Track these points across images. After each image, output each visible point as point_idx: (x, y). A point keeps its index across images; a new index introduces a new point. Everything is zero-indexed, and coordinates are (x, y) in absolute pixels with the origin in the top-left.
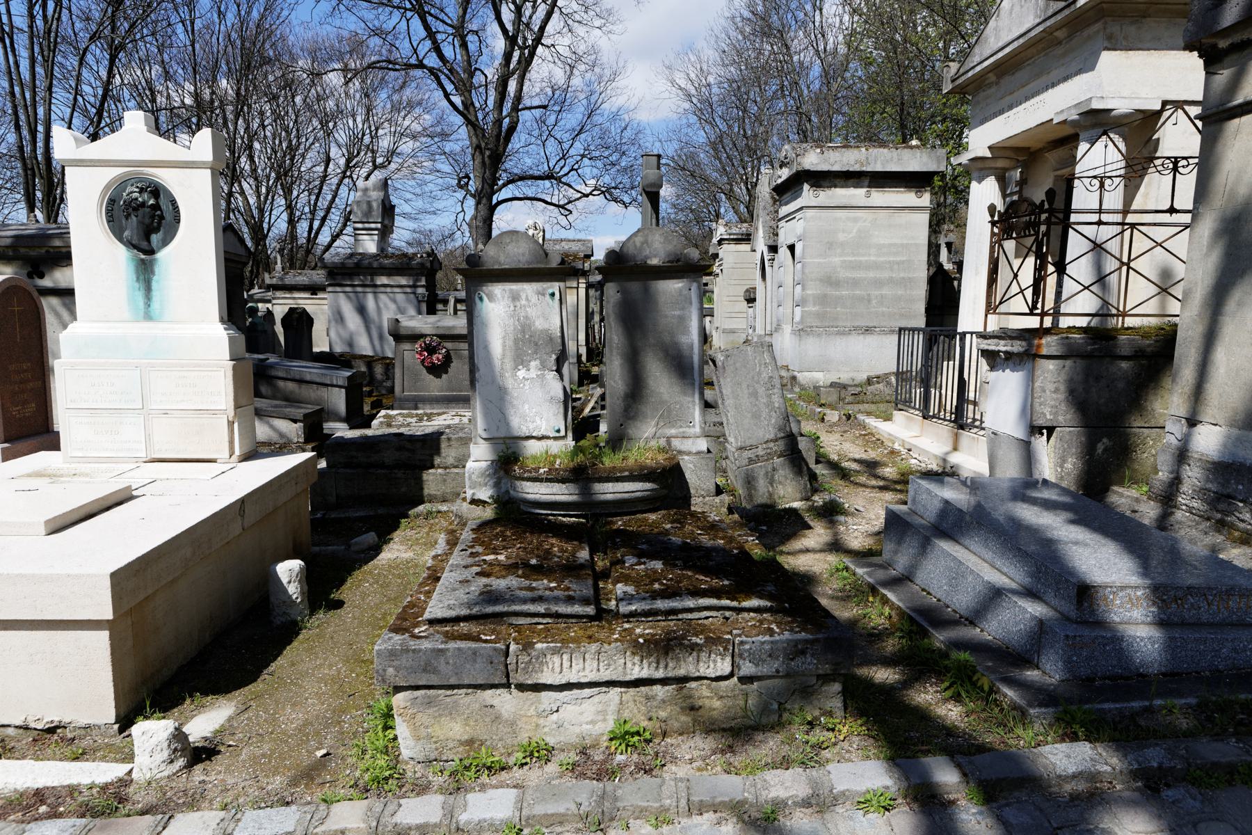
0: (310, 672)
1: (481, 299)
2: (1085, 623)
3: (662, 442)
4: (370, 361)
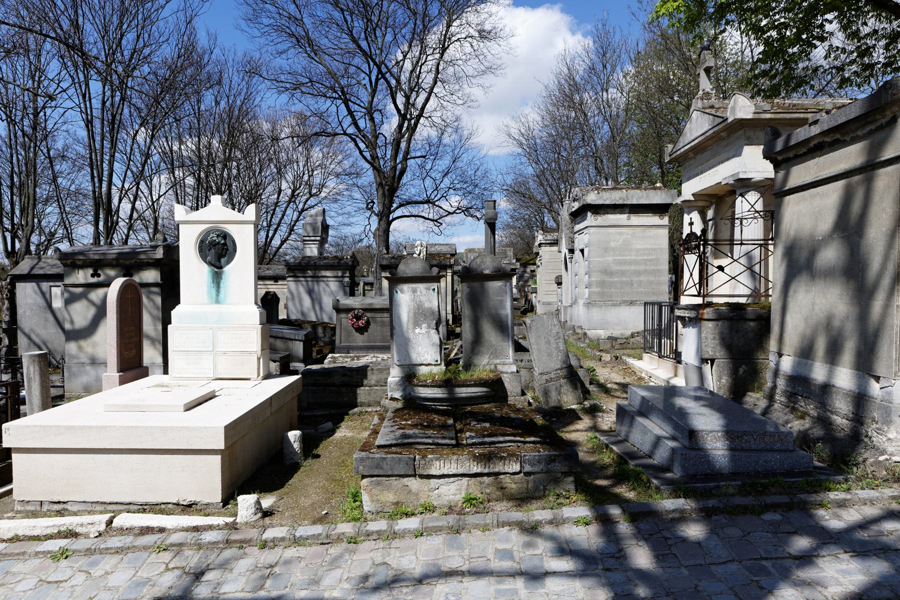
0: (309, 483)
2: (694, 449)
3: (492, 367)
4: (314, 325)
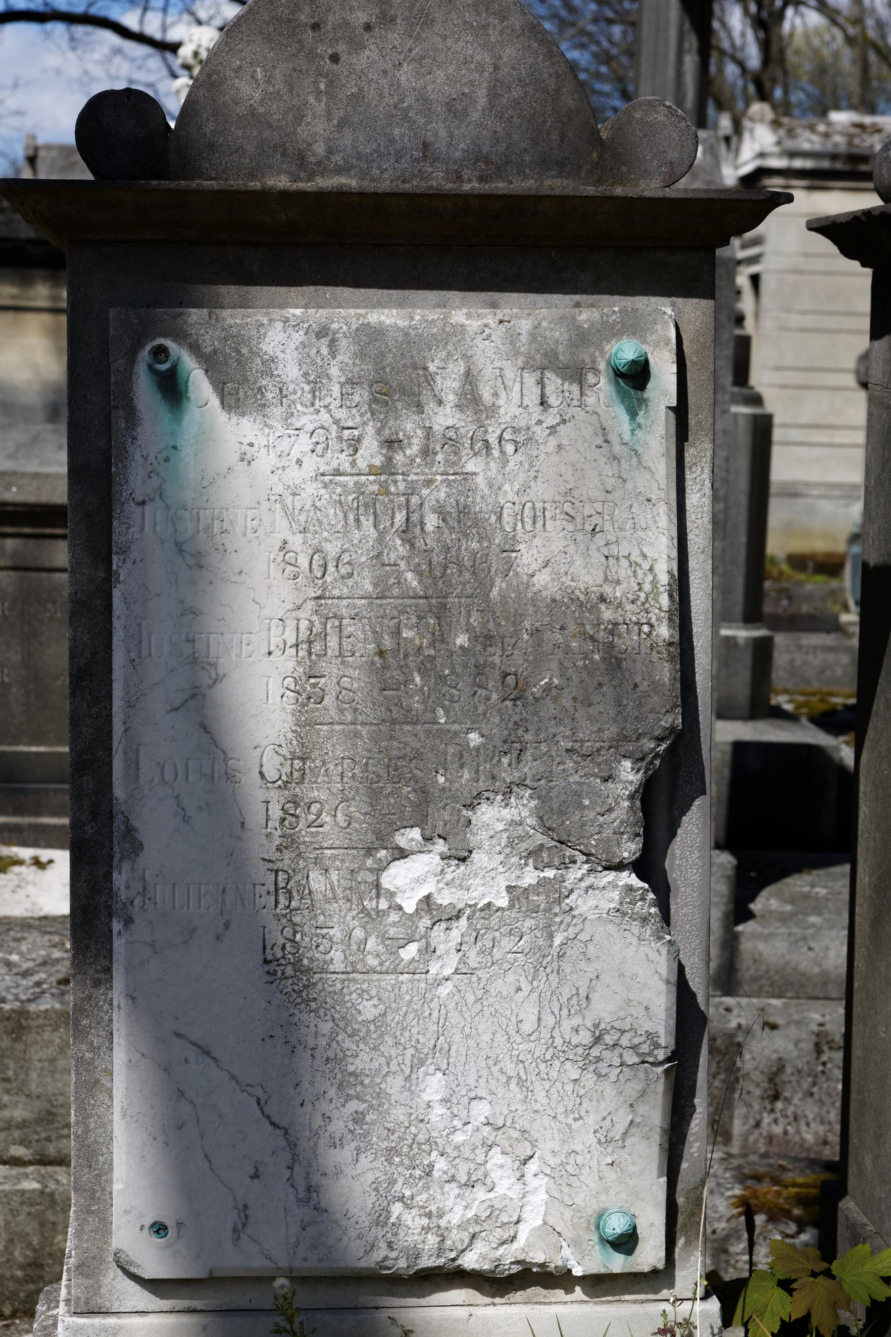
1: (172, 388)
